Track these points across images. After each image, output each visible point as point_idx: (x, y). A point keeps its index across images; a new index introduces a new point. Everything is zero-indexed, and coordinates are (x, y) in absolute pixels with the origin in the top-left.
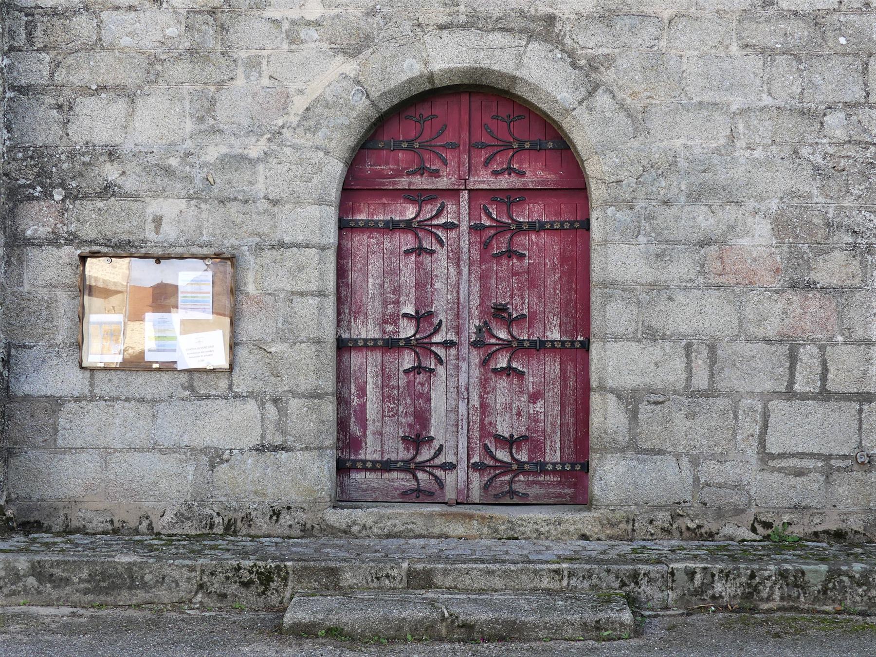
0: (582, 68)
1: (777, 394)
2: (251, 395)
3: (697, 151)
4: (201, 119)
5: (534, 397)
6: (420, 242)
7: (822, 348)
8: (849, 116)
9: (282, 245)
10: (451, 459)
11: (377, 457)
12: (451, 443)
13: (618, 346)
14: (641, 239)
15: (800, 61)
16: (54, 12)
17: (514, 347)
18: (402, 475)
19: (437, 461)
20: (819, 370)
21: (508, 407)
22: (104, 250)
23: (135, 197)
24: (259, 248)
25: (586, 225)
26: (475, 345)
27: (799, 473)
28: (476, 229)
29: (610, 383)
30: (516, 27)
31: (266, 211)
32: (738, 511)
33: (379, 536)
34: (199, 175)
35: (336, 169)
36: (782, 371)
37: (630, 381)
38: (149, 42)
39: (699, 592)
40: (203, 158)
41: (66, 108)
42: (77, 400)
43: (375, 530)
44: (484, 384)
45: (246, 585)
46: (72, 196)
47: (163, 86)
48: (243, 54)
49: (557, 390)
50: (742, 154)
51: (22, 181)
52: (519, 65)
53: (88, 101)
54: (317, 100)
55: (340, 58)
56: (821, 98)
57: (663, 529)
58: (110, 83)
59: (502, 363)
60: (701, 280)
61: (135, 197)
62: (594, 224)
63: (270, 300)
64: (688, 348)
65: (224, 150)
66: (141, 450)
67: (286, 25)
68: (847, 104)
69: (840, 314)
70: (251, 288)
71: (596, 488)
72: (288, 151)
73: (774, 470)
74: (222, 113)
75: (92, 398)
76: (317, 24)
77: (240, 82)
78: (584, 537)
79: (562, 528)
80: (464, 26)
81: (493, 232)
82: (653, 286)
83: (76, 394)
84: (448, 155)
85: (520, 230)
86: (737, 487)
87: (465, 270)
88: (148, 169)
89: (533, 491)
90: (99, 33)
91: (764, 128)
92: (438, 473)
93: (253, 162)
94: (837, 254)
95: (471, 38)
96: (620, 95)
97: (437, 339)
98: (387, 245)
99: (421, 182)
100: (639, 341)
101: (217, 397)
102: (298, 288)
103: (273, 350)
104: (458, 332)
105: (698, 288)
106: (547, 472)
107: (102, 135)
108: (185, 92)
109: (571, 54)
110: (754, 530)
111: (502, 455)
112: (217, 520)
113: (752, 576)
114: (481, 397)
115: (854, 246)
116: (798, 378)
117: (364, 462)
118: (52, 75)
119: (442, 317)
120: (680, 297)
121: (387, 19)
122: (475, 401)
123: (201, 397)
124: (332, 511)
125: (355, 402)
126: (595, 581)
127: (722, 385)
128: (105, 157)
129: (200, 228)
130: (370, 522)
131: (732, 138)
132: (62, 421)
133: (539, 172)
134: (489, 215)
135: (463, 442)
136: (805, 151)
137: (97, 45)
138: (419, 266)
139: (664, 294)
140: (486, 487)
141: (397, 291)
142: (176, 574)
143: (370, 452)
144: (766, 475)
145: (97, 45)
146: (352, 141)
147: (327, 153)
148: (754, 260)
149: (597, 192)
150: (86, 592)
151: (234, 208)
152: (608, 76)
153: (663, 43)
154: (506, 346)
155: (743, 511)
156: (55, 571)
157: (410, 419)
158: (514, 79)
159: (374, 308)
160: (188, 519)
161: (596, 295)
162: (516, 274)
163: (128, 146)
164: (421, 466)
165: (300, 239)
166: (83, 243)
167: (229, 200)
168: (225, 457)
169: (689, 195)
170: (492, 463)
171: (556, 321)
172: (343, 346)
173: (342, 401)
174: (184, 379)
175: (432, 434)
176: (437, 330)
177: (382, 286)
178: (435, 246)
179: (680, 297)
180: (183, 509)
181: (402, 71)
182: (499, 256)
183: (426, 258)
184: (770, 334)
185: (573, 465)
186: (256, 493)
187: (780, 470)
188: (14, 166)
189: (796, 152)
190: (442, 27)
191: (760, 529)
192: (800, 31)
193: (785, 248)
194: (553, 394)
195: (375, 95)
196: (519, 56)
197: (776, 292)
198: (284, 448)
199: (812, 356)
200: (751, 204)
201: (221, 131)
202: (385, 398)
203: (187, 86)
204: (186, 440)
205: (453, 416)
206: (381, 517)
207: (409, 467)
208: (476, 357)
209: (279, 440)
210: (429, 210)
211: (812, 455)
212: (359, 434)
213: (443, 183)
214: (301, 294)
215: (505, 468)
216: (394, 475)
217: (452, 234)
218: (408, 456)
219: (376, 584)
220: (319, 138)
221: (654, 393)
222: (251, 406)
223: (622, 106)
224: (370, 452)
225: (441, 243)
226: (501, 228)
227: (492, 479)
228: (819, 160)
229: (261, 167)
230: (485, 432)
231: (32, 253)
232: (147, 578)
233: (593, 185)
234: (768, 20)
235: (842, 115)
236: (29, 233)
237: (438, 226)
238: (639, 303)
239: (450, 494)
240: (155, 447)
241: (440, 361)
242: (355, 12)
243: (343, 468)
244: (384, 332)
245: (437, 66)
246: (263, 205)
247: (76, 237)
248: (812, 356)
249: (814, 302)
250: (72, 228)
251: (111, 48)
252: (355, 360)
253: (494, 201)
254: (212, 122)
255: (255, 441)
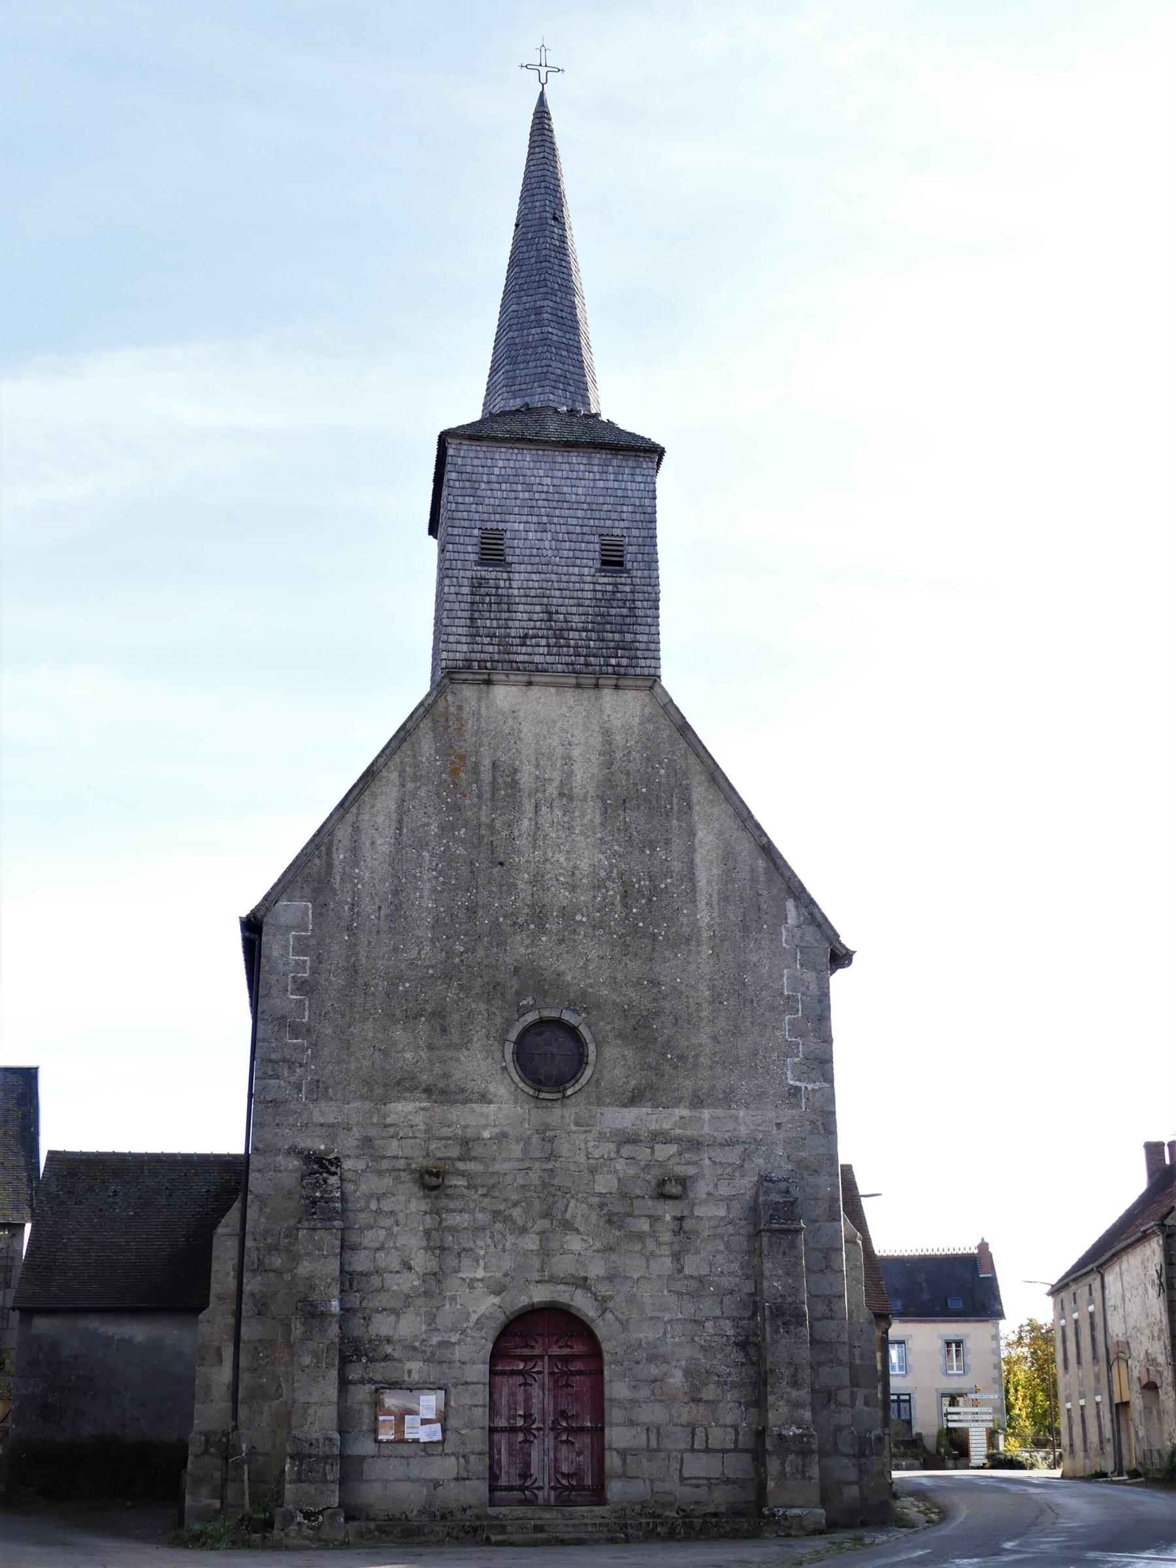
0: (599, 1301)
1: (686, 1450)
2: (453, 1454)
3: (650, 1339)
4: (430, 1324)
5: (579, 1454)
6: (526, 1379)
7: (706, 1428)
8: (715, 1323)
9: (467, 1383)
10: (541, 1484)
11: (507, 1484)
12: (541, 1477)
13: (617, 1429)
14: (627, 1379)
15: (694, 1298)
16: (362, 1274)
17: (570, 1430)
18: (518, 1493)
19: (535, 1486)
20: (705, 1439)
21: (567, 1459)
22: (385, 1386)
23: (400, 1361)
24: (456, 1385)
25: (602, 1372)
26: (551, 1429)
27: (697, 1486)
28: (551, 1374)
29: (614, 1446)
30: (570, 1281)
31: (459, 1367)
32: (671, 1505)
33: (511, 1519)
34: (429, 1350)
35: (490, 1346)
36: (689, 1440)
37: (623, 1445)
38: (406, 1289)
39: (651, 1531)
40: (431, 1342)
41: (367, 1319)
42: (373, 1457)
43: (510, 1517)
44: (556, 1449)
45: (467, 1533)
46: (370, 1360)
47: (412, 1309)
48: (448, 1294)
49: (589, 1450)
50: (669, 1340)
51: (347, 1354)
52: (572, 1300)
53: (378, 1315)
54: (482, 1315)
55: (492, 1296)
56: (703, 1315)
57: (638, 1514)
58: (388, 1307)
59: (564, 1438)
60: (653, 1398)
61: (400, 1361)
62: (606, 1372)
63: (461, 1409)
64: (648, 1429)
65: (440, 1338)
66: (402, 1481)
67: (468, 1281)
68: (714, 1317)
69: (713, 1413)
70: (452, 1403)
71: (608, 1496)
72: (469, 1339)
73: (686, 1485)
74: (439, 1322)
75: (379, 1456)
76: (482, 1280)
77: (447, 1307)
78: (603, 1518)
79: (593, 1514)
80: (547, 1281)
81: (559, 1375)
82: (633, 1401)
83: (372, 1454)
84: (539, 1339)
85: (572, 1374)
86: (670, 1493)
87: (547, 1393)
88: (405, 1347)
89: (579, 1499)
90: (383, 1284)
91: (679, 1328)
92: (535, 1491)
93: (453, 1344)
94: (711, 1385)
95: (551, 1287)
96: (616, 1313)
97: (534, 1426)
98: (511, 1381)
99: (526, 1352)
100: (626, 1426)
101: (437, 1455)
102: (474, 1403)
103: (462, 1432)
104: (544, 1424)
105: (651, 1401)
106: (585, 1490)
107: (385, 1331)
108: (422, 1312)
109: (595, 1294)
110: (678, 1513)
111: (564, 1482)
112: (438, 1513)
113: (672, 1524)
114: (554, 1454)
115: (718, 1382)
116: (696, 1442)
117: (501, 1486)
118: (361, 1303)
119: (536, 1416)
120: (644, 1406)
121: (513, 1278)
122: (552, 1456)
123: (429, 1455)
124: (489, 1508)
125: (496, 1457)
126: (609, 1528)
127: (663, 1446)
128: (385, 1342)
129: (429, 1375)
130: (507, 1513)
131: (665, 1333)
132: (365, 1467)
133: (580, 1347)
134: (557, 1367)
135: (546, 1475)
136: (696, 1339)
137: (382, 1289)
138: (525, 1391)
139: (637, 1404)
140: (557, 1498)
141: (515, 1403)
142: (437, 1529)
143: (503, 1481)
144: (683, 1487)
145: (382, 1289)
146: (497, 1334)
147: (486, 1340)
148: (676, 1389)
149: (607, 1358)
150: (400, 1538)
151: (445, 1366)
152: (611, 1304)
153: (635, 1290)
154: (565, 1429)
155: (673, 1505)
156: (387, 1528)
157: (521, 1465)
158: (570, 1306)
159: (504, 1411)
160: (424, 1513)
161: (607, 1405)
162: (571, 1395)
163: (396, 1337)
164: (527, 1488)
165: (475, 1380)
166: (375, 1382)
167: (443, 1362)
168: (441, 1483)
169: (647, 1359)
170: (560, 1486)
171: (588, 1417)
172: (492, 1430)
173: (491, 1457)
174: (422, 1446)
175: (532, 1472)
176: (534, 1422)
177: (508, 1401)
178: (533, 1382)
179: (644, 1406)
180: (422, 1508)
181: (520, 1302)
182: (562, 1386)
183: (529, 1388)
184: (683, 1423)
185: (597, 1486)
186: (455, 1500)
187: (689, 1485)
188: (343, 1346)
189: (693, 1339)
190: (537, 1282)
191: (680, 1513)
192: (694, 1285)
193: (689, 1383)
194: (587, 1452)
195: (508, 1314)
196: (572, 1296)
197: (685, 1403)
198: (469, 1479)
199: (701, 1432)
200: (674, 1363)
201: (439, 1330)
202: (510, 1455)
203: (423, 1309)
204: (423, 1476)
205: (541, 1463)
206: (512, 1510)
207: (521, 1489)
208: (552, 1435)
209: (465, 1475)
210: (530, 1365)
211: (703, 1478)
212: (498, 1473)
213: (537, 1352)
214: (476, 1406)
215: (565, 1488)
216: (515, 1493)
217: (540, 1376)
218: (521, 1483)
219: (521, 1531)
220: (483, 1334)
221: (633, 1450)
222: (453, 1459)
223: (617, 1318)
224: (503, 1481)
225: (535, 1381)
226: (563, 1373)
227: (560, 1494)
228: (703, 1342)
229: (457, 1347)
230: (557, 1470)
231: (352, 1387)
232: (426, 1530)
233: (605, 1354)
234: (680, 1279)
235: (712, 1322)
236: (350, 1377)
237: (534, 1372)
238: (626, 1409)
239: (541, 1501)
240: (408, 1479)
241: (535, 1437)
242: (499, 1275)
243: (492, 1489)
244: (509, 1423)
245: (536, 1300)
246: (458, 1364)
247: (372, 1379)
248: (701, 1432)
249: (702, 1408)
250: (370, 1375)
251: (388, 1291)
252: (496, 1436)
253: (560, 1360)
254: (434, 1325)
255: (454, 1476)
